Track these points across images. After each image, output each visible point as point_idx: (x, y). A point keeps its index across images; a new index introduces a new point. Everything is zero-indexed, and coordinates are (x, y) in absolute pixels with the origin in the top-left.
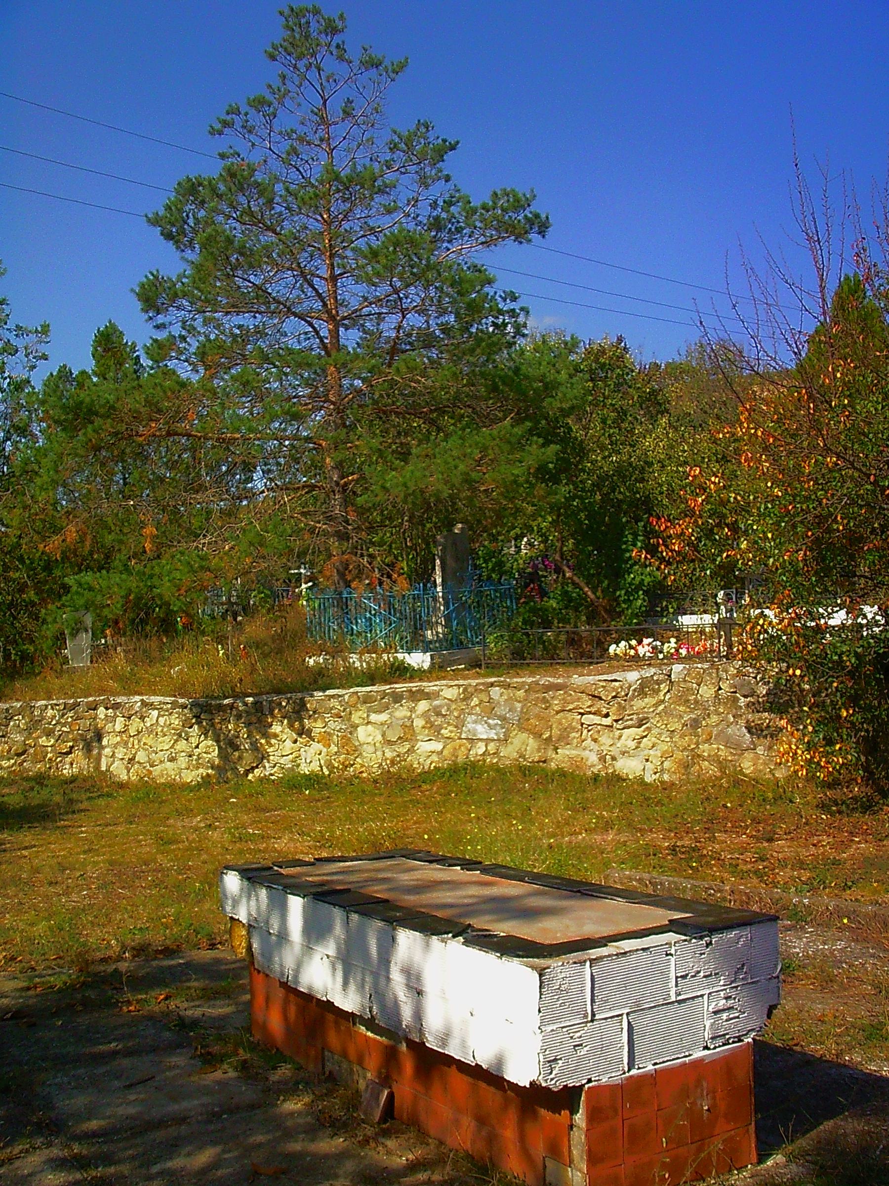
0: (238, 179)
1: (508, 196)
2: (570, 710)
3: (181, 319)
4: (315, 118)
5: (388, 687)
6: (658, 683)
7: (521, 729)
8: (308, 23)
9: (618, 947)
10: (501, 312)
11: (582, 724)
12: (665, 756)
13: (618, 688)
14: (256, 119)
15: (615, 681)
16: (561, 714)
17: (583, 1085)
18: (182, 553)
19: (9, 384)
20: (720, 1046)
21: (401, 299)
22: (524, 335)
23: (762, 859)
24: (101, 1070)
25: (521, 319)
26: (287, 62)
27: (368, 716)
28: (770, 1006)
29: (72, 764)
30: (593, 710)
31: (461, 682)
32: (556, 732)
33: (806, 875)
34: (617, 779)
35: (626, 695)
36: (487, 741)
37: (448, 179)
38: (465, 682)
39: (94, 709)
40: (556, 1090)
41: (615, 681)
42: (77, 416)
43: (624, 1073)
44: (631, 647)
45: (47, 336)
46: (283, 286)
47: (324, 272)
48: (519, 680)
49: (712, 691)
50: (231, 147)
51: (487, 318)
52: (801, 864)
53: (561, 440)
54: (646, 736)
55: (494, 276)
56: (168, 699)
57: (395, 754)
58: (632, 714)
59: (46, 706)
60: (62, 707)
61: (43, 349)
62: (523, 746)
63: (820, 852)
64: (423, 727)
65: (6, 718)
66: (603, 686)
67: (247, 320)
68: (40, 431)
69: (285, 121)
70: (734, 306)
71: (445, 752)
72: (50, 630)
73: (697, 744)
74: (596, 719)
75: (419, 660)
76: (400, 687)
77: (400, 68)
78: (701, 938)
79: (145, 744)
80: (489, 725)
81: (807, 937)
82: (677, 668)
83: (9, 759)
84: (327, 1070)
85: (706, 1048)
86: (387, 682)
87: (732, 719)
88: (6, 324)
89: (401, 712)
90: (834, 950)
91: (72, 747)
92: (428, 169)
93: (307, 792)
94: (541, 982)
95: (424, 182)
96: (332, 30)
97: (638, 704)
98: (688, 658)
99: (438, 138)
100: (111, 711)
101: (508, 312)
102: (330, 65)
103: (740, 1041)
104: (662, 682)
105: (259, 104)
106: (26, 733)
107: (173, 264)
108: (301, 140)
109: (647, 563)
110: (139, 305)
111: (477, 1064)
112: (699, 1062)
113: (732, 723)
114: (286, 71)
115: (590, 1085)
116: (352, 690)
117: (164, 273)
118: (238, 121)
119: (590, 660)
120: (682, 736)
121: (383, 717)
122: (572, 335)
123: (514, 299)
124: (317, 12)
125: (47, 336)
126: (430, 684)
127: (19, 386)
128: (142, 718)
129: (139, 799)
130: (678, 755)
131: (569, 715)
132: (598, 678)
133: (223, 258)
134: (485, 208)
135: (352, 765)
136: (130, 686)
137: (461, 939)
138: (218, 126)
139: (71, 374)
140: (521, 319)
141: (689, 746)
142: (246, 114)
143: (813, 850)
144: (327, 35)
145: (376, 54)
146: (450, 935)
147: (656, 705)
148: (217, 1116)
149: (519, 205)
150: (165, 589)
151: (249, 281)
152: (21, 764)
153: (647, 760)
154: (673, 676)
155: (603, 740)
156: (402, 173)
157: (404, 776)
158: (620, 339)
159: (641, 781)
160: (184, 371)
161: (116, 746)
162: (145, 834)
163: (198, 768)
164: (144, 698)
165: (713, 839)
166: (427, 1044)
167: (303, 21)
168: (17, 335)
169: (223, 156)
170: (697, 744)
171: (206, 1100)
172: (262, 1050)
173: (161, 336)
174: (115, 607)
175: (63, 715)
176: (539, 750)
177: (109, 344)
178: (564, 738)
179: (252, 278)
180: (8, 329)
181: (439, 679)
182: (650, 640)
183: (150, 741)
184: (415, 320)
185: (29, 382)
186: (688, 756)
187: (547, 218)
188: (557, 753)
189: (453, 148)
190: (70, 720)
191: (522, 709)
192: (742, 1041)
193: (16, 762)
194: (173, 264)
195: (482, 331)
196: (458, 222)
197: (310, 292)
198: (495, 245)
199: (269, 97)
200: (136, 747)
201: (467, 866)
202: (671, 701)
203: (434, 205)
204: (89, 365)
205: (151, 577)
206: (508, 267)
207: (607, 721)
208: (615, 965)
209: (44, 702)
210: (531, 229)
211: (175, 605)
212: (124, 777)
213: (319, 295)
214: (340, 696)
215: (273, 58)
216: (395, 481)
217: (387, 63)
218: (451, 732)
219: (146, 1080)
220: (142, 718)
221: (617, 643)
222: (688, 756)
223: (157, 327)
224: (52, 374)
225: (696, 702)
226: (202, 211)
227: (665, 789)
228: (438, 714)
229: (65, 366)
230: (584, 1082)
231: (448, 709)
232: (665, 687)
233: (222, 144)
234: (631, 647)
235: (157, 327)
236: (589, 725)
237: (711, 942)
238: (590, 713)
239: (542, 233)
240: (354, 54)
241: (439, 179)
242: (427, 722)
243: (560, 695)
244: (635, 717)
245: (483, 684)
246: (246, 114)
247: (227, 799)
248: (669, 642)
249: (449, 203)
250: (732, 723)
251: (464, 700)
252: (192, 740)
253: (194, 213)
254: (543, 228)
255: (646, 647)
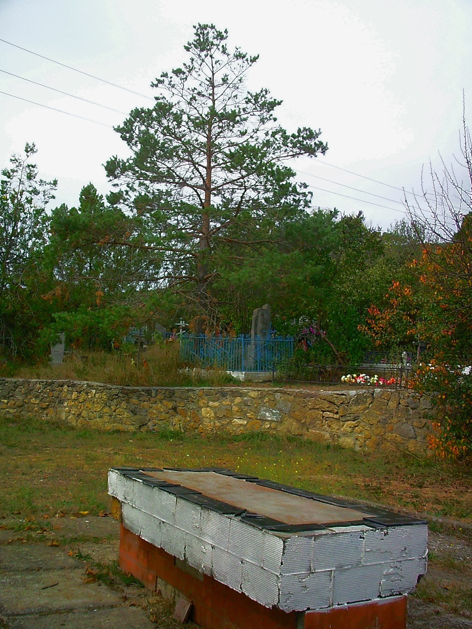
0: (163, 109)
1: (306, 131)
2: (317, 409)
3: (127, 182)
4: (208, 83)
5: (220, 388)
6: (366, 397)
7: (290, 417)
8: (208, 33)
9: (332, 530)
10: (299, 194)
11: (323, 417)
12: (367, 438)
13: (344, 399)
14: (176, 80)
15: (343, 395)
16: (312, 410)
17: (305, 611)
18: (116, 306)
19: (34, 210)
20: (388, 596)
21: (245, 182)
22: (309, 207)
23: (417, 497)
24: (30, 577)
25: (308, 198)
26: (195, 53)
27: (208, 403)
28: (420, 575)
29: (47, 414)
30: (330, 409)
31: (260, 389)
32: (308, 420)
33: (440, 507)
34: (339, 448)
35: (349, 403)
36: (272, 421)
37: (275, 120)
38: (262, 389)
39: (62, 386)
40: (288, 612)
41: (343, 395)
42: (67, 229)
43: (329, 607)
44: (353, 378)
45: (56, 186)
46: (184, 170)
47: (205, 164)
48: (291, 390)
49: (395, 405)
50: (161, 94)
51: (290, 196)
52: (438, 501)
53: (325, 264)
54: (357, 426)
55: (295, 173)
56: (102, 385)
57: (220, 424)
58: (351, 414)
59: (37, 382)
60: (44, 383)
61: (53, 193)
62: (291, 426)
63: (449, 495)
64: (237, 411)
65: (14, 386)
66: (336, 397)
67: (163, 187)
68: (48, 238)
69: (191, 83)
70: (425, 194)
71: (248, 426)
72: (41, 341)
73: (385, 433)
74: (331, 415)
75: (238, 375)
76: (227, 389)
77: (254, 60)
78: (382, 530)
79: (87, 407)
80: (273, 413)
81: (440, 541)
82: (378, 390)
83: (14, 409)
84: (158, 589)
85: (380, 596)
86: (220, 385)
87: (405, 421)
88: (35, 178)
89: (226, 402)
90: (455, 549)
91: (48, 405)
92: (265, 114)
93: (171, 440)
94: (285, 546)
95: (263, 121)
96: (220, 36)
97: (355, 408)
98: (382, 387)
99: (272, 98)
100: (70, 388)
101: (302, 194)
102: (218, 55)
103: (400, 594)
104: (369, 397)
105: (178, 72)
106: (24, 396)
107: (126, 153)
108: (199, 94)
109: (366, 333)
110: (106, 173)
111: (242, 592)
112: (374, 605)
113: (404, 423)
114: (194, 57)
115: (308, 612)
116: (200, 388)
117: (120, 158)
118: (166, 81)
119: (330, 383)
120: (377, 428)
121: (216, 404)
122: (335, 208)
123: (306, 186)
124: (213, 27)
125: (56, 186)
126: (242, 388)
127: (39, 212)
128: (87, 393)
129: (80, 436)
130: (374, 438)
131: (316, 411)
132: (333, 392)
133: (149, 146)
134: (293, 136)
135: (197, 428)
136: (82, 374)
137: (240, 518)
138: (156, 82)
139: (67, 209)
140: (308, 198)
141: (380, 433)
142: (171, 78)
143: (445, 494)
144: (218, 40)
145: (243, 51)
146: (234, 515)
147: (364, 410)
148: (90, 609)
149: (311, 135)
150: (104, 325)
151: (165, 165)
152: (20, 412)
153: (357, 439)
154: (374, 395)
155: (334, 426)
156: (251, 115)
157: (224, 436)
158: (360, 213)
159: (352, 450)
160: (128, 212)
161: (71, 407)
162: (80, 454)
163: (114, 423)
164: (89, 382)
165: (389, 484)
166: (215, 579)
167: (206, 32)
168: (40, 185)
169: (157, 99)
170: (385, 433)
171: (86, 600)
172: (123, 575)
173: (116, 190)
174: (77, 333)
175: (45, 388)
176: (298, 429)
177: (88, 194)
178: (312, 424)
179: (166, 163)
180: (35, 182)
181: (248, 386)
182: (364, 375)
183: (90, 406)
184: (251, 194)
185: (44, 210)
186: (379, 439)
187: (327, 144)
188: (308, 431)
189: (279, 103)
190: (48, 391)
191: (291, 406)
192: (402, 594)
193: (17, 411)
194: (126, 153)
195: (287, 203)
196: (279, 143)
197: (197, 174)
198: (298, 157)
199: (184, 69)
200: (82, 408)
201: (249, 480)
202: (372, 408)
203: (267, 134)
204: (77, 205)
205: (98, 317)
206: (303, 169)
207: (335, 416)
208: (331, 541)
209: (35, 380)
210: (318, 150)
211: (109, 334)
212: (74, 423)
213: (201, 176)
214: (194, 390)
215: (188, 49)
216: (234, 277)
217: (248, 57)
218: (252, 415)
219: (53, 586)
220: (87, 393)
221: (346, 375)
222: (379, 439)
223: (114, 185)
224: (57, 208)
225: (386, 410)
226: (143, 126)
227: (365, 455)
228: (246, 405)
229: (64, 204)
230: (305, 609)
231: (251, 403)
232: (369, 401)
233: (157, 92)
234: (353, 378)
235: (114, 185)
236: (327, 418)
237: (387, 532)
238: (328, 411)
239: (323, 152)
240: (231, 50)
241: (270, 119)
242: (239, 409)
243: (313, 400)
244: (352, 415)
245: (271, 390)
246: (171, 78)
247: (127, 440)
248: (374, 377)
249: (274, 134)
250: (404, 423)
251: (260, 398)
252: (113, 407)
253: (139, 128)
254: (324, 149)
255: (361, 379)
